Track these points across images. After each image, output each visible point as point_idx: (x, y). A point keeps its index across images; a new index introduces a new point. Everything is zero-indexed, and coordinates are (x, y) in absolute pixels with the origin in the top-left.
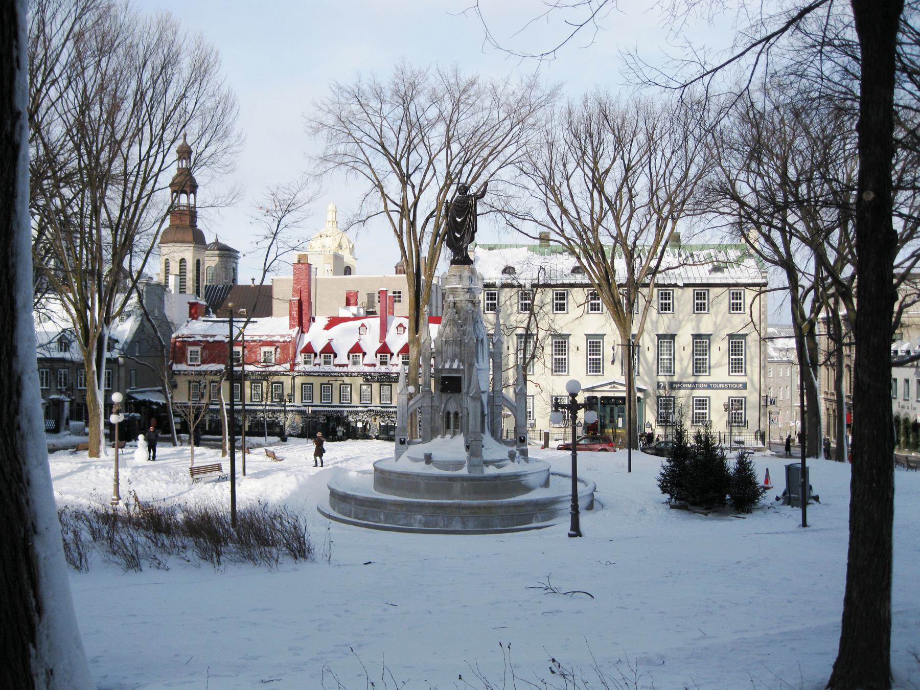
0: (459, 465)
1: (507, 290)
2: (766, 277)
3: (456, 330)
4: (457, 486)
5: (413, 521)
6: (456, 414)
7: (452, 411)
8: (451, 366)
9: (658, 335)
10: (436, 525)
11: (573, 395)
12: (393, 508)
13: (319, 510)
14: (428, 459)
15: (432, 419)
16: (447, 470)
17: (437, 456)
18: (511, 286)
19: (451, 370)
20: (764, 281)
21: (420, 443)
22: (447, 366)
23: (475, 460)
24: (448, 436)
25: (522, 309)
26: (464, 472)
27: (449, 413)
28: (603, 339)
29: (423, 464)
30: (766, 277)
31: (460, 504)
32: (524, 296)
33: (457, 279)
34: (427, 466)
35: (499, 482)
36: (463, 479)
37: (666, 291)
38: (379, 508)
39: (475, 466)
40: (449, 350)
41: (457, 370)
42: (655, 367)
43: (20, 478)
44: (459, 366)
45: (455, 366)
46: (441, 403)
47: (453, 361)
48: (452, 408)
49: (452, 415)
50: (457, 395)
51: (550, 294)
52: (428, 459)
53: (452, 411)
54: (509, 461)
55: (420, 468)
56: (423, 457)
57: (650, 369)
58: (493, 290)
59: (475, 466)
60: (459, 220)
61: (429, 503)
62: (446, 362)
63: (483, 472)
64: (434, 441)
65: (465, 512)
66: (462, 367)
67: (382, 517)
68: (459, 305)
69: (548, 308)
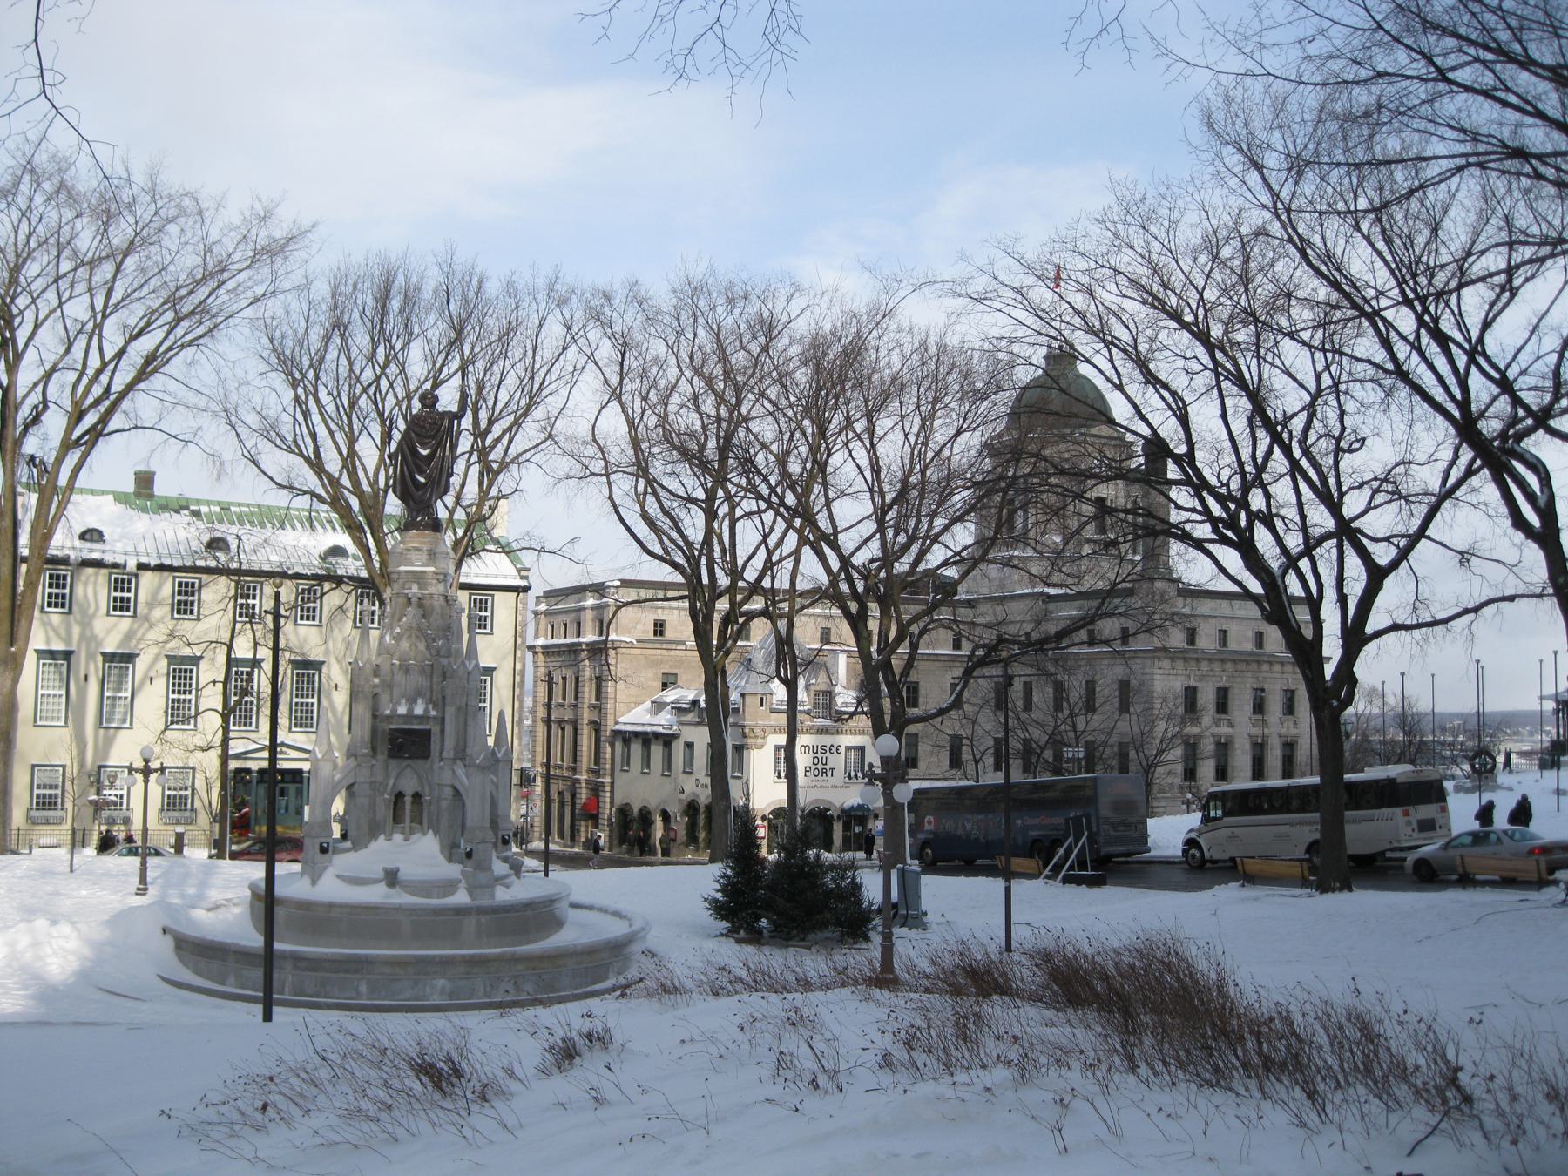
0: (449, 887)
1: (90, 570)
2: (526, 578)
3: (422, 646)
4: (470, 924)
5: (428, 990)
6: (417, 796)
7: (409, 792)
8: (410, 710)
9: (103, 654)
10: (359, 996)
11: (147, 761)
12: (387, 970)
13: (163, 979)
14: (392, 878)
15: (372, 807)
16: (428, 896)
17: (407, 871)
18: (98, 564)
19: (410, 717)
20: (523, 583)
21: (348, 850)
22: (402, 710)
23: (482, 877)
24: (398, 837)
25: (115, 609)
26: (461, 897)
27: (399, 796)
28: (197, 665)
29: (382, 888)
30: (526, 578)
31: (513, 954)
32: (120, 585)
33: (425, 557)
34: (392, 891)
35: (530, 913)
36: (460, 911)
37: (122, 580)
38: (356, 971)
39: (482, 887)
40: (416, 680)
41: (423, 718)
42: (347, 718)
43: (787, 940)
44: (426, 710)
45: (419, 710)
46: (387, 776)
47: (412, 701)
48: (409, 785)
49: (408, 800)
50: (420, 763)
51: (168, 585)
52: (392, 878)
53: (409, 792)
54: (514, 878)
55: (376, 894)
56: (381, 874)
57: (339, 722)
58: (62, 570)
59: (482, 887)
60: (424, 453)
61: (463, 956)
62: (399, 703)
63: (492, 896)
64: (373, 846)
65: (520, 967)
66: (433, 713)
67: (363, 988)
68: (427, 602)
69: (161, 612)
